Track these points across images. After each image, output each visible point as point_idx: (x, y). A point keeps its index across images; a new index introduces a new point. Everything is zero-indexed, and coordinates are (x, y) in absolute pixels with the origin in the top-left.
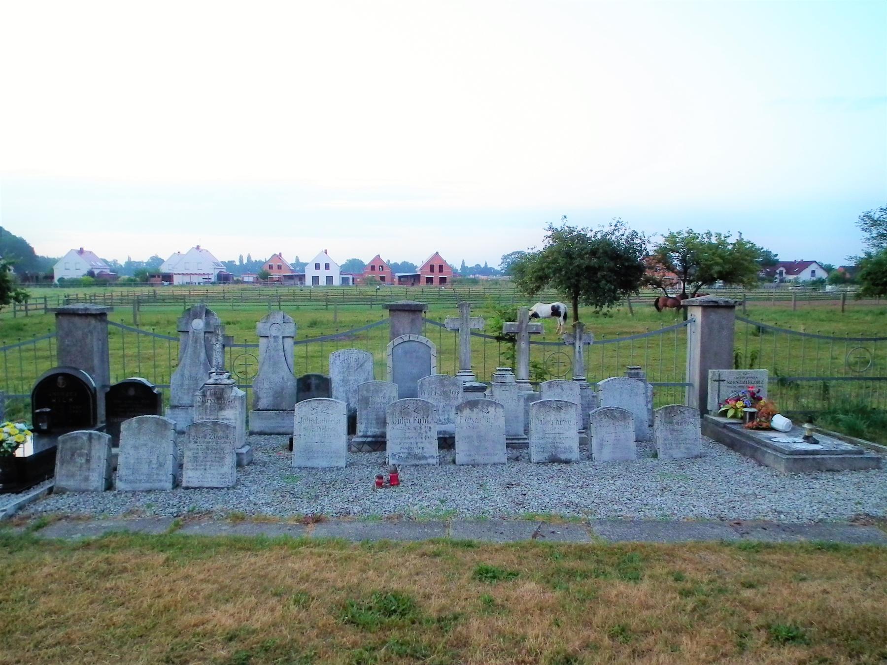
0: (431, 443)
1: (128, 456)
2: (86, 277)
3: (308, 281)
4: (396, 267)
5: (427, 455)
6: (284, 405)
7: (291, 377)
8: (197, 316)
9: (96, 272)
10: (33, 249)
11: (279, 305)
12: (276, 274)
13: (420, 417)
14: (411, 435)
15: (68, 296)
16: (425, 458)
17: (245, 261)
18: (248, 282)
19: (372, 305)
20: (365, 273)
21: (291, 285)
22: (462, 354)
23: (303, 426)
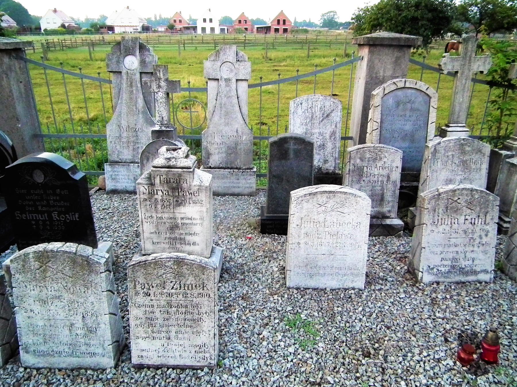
0: (485, 252)
1: (31, 314)
2: (60, 29)
3: (199, 31)
4: (254, 22)
5: (478, 269)
6: (238, 163)
7: (247, 130)
8: (129, 52)
9: (66, 25)
10: (27, 10)
11: (184, 47)
12: (178, 26)
13: (474, 216)
14: (459, 241)
15: (47, 40)
16: (475, 273)
17: (158, 18)
18: (161, 32)
19: (245, 46)
20: (235, 25)
21: (188, 34)
22: (457, 105)
23: (303, 231)
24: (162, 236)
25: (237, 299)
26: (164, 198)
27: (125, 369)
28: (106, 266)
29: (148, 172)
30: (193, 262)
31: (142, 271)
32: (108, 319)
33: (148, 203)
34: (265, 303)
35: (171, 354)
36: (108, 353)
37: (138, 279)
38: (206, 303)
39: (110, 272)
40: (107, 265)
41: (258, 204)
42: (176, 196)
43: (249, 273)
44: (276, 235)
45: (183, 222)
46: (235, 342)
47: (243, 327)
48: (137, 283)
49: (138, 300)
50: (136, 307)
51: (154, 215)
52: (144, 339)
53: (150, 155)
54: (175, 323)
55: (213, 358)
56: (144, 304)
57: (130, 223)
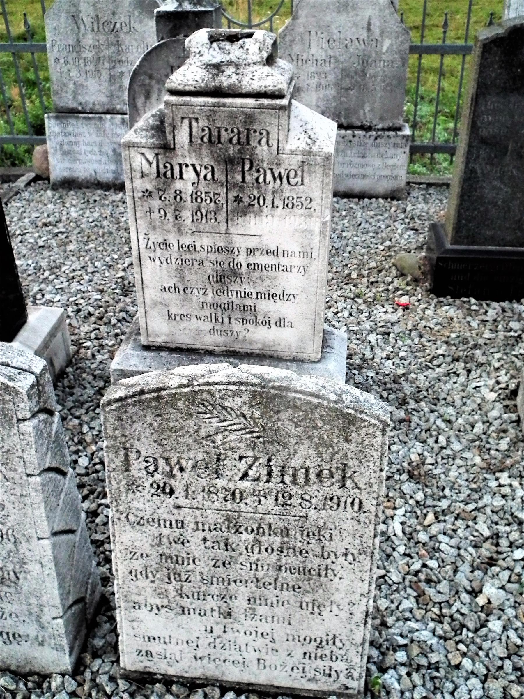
24: (194, 299)
25: (397, 477)
26: (202, 188)
27: (103, 679)
28: (35, 400)
29: (154, 111)
30: (315, 401)
31: (149, 420)
32: (49, 552)
33: (156, 203)
34: (476, 496)
35: (233, 655)
36: (52, 637)
37: (136, 443)
38: (349, 525)
39: (51, 413)
40: (40, 394)
41: (412, 218)
42: (235, 185)
43: (417, 402)
44: (473, 301)
45: (252, 260)
46: (408, 615)
47: (424, 565)
48: (133, 456)
49: (135, 504)
50: (132, 525)
51: (172, 239)
52: (155, 611)
53: (153, 82)
54: (246, 574)
55: (356, 675)
56: (156, 516)
57: (108, 259)
